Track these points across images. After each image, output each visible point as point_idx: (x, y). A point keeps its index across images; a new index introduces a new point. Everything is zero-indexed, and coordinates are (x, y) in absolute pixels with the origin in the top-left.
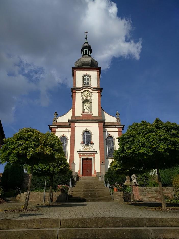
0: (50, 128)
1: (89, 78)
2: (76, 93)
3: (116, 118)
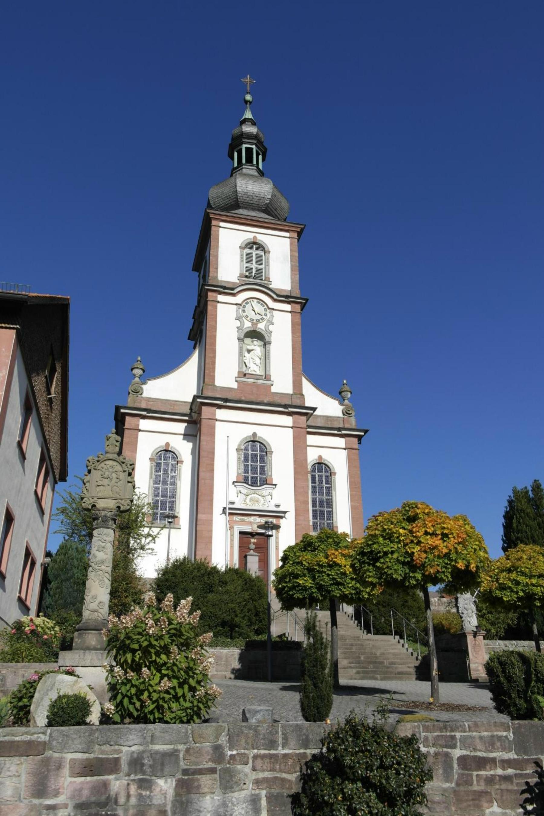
0: (116, 418)
3: (341, 404)
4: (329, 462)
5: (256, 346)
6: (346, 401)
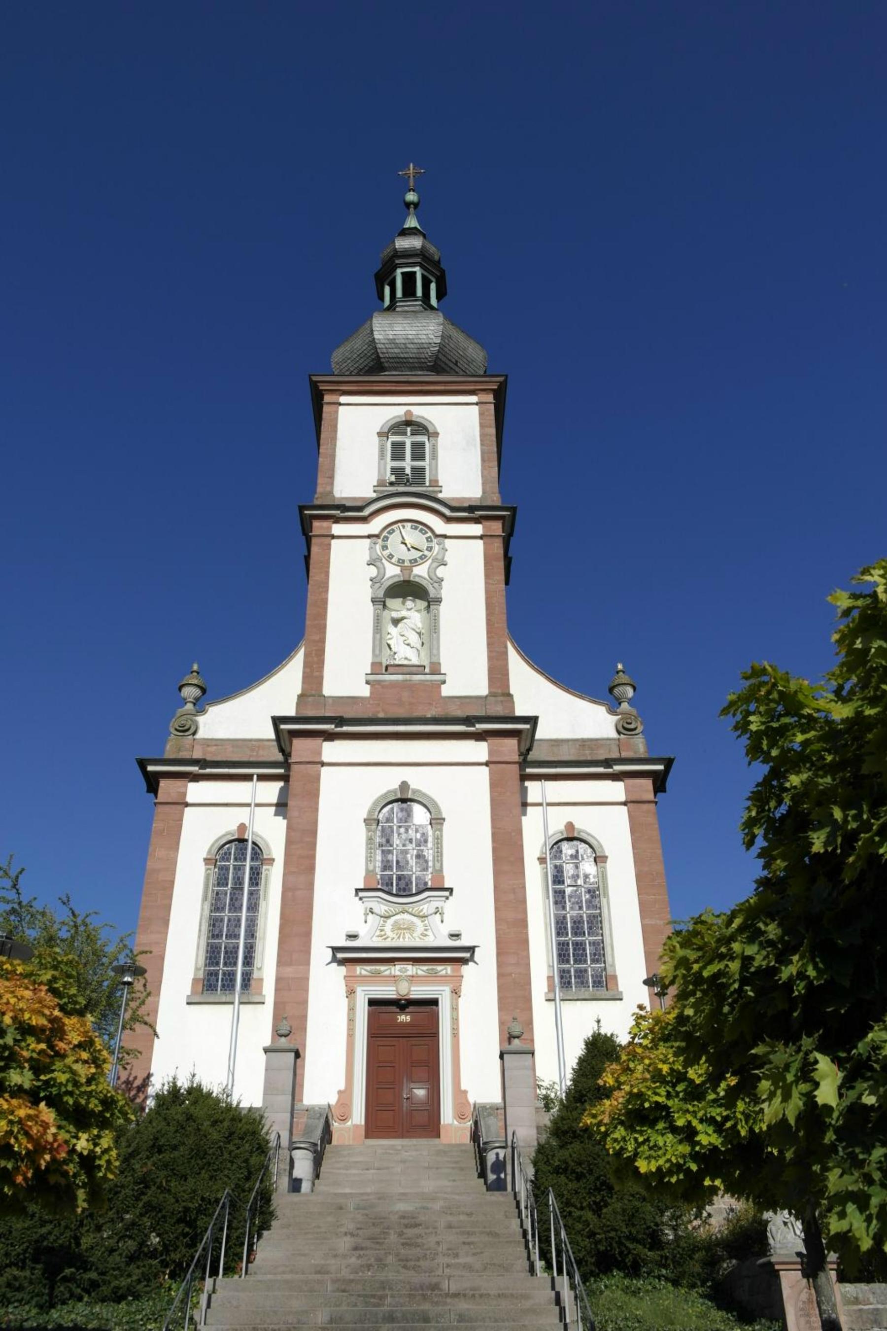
1: (427, 445)
2: (333, 537)
3: (612, 711)
4: (589, 834)
5: (412, 613)
6: (625, 706)
